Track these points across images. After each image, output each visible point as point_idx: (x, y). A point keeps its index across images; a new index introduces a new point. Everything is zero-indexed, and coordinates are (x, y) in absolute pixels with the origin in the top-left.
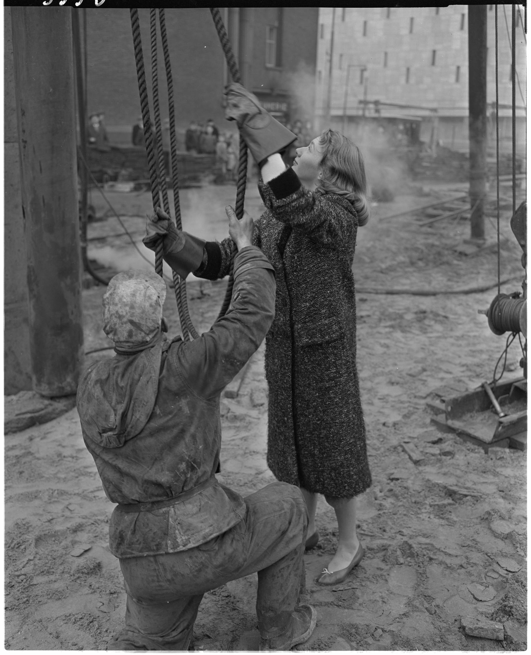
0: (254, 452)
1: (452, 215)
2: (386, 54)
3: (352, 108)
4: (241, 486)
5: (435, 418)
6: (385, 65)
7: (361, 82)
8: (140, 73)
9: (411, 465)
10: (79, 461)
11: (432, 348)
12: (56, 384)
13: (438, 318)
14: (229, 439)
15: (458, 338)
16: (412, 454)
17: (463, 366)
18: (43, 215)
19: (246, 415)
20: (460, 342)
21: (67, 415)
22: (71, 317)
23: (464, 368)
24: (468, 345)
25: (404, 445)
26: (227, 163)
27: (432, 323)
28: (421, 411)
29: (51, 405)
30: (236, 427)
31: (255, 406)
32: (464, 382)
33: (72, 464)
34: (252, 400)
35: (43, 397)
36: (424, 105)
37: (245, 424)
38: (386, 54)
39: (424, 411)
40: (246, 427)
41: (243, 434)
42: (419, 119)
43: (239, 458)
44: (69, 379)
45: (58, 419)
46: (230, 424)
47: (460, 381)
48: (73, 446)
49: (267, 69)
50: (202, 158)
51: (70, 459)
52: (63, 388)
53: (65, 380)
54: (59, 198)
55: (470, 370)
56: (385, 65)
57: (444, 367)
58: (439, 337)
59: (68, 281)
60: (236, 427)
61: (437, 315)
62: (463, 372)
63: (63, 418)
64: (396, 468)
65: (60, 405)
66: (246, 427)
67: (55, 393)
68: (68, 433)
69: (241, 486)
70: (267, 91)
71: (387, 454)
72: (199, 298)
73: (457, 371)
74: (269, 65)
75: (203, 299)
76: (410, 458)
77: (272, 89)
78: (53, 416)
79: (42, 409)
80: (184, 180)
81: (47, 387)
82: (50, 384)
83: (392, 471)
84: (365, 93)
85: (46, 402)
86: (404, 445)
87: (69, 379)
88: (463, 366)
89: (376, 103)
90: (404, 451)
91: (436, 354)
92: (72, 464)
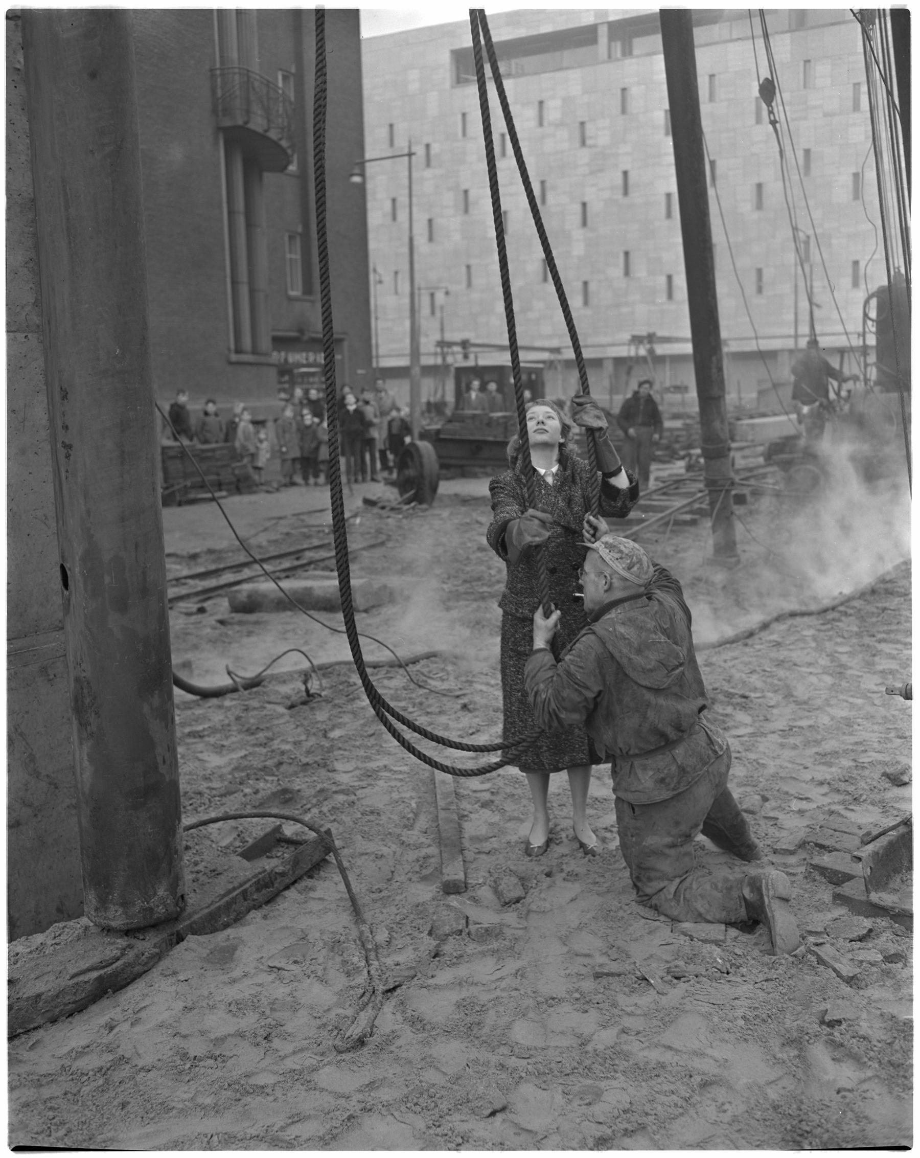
0: (553, 999)
1: (662, 518)
2: (468, 267)
3: (429, 354)
4: (567, 1075)
5: (839, 890)
6: (469, 284)
7: (433, 313)
8: (326, 315)
9: (846, 989)
10: (229, 1063)
11: (752, 756)
12: (139, 904)
13: (734, 701)
14: (494, 978)
15: (784, 733)
16: (837, 966)
17: (821, 783)
18: (107, 579)
19: (501, 925)
20: (792, 740)
21: (164, 964)
22: (163, 769)
23: (825, 789)
24: (807, 744)
25: (815, 949)
26: (253, 456)
27: (729, 710)
28: (800, 877)
29: (130, 947)
30: (494, 952)
31: (507, 904)
32: (839, 814)
33: (219, 1073)
34: (496, 891)
35: (108, 930)
36: (538, 344)
37: (507, 943)
38: (468, 267)
39: (806, 878)
40: (512, 948)
41: (512, 965)
42: (541, 366)
43: (531, 1015)
44: (161, 892)
45: (147, 978)
46: (480, 949)
47: (832, 813)
48: (202, 1033)
49: (291, 299)
50: (213, 450)
51: (210, 1062)
52: (151, 910)
53: (155, 894)
54: (137, 546)
55: (838, 791)
56: (469, 284)
57: (791, 787)
58: (753, 735)
59: (156, 701)
60: (494, 952)
61: (730, 695)
62: (824, 795)
63: (155, 973)
64: (825, 999)
65: (147, 945)
66: (512, 948)
67: (136, 922)
68: (181, 1005)
69: (567, 1075)
70: (294, 334)
71: (794, 971)
72: (304, 703)
73: (819, 797)
74: (293, 293)
75: (312, 705)
76: (839, 975)
77: (301, 331)
78: (138, 969)
79: (118, 959)
80: (186, 490)
81: (120, 911)
82: (125, 904)
83: (822, 1007)
84: (442, 330)
85: (122, 942)
86: (815, 949)
87: (161, 892)
88: (821, 783)
89: (465, 344)
90: (821, 961)
91: (764, 766)
92: (219, 1073)
